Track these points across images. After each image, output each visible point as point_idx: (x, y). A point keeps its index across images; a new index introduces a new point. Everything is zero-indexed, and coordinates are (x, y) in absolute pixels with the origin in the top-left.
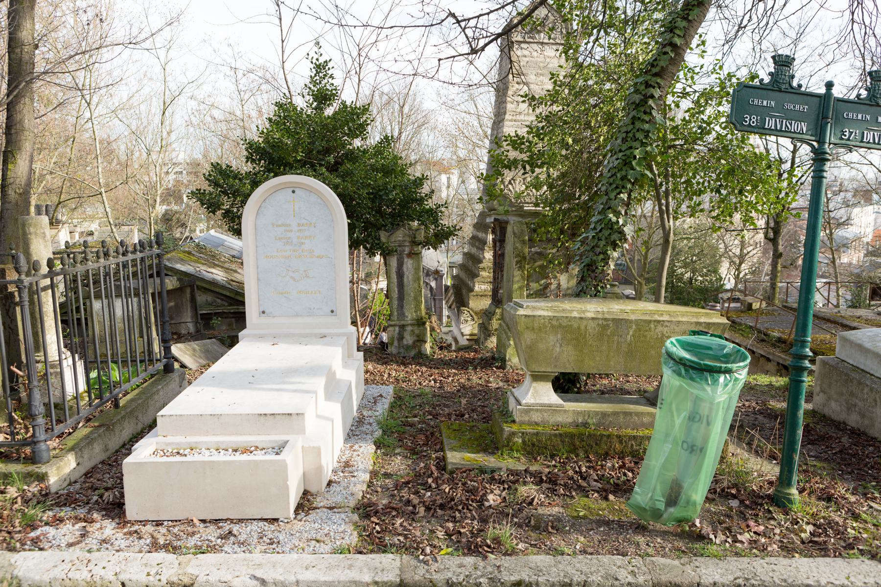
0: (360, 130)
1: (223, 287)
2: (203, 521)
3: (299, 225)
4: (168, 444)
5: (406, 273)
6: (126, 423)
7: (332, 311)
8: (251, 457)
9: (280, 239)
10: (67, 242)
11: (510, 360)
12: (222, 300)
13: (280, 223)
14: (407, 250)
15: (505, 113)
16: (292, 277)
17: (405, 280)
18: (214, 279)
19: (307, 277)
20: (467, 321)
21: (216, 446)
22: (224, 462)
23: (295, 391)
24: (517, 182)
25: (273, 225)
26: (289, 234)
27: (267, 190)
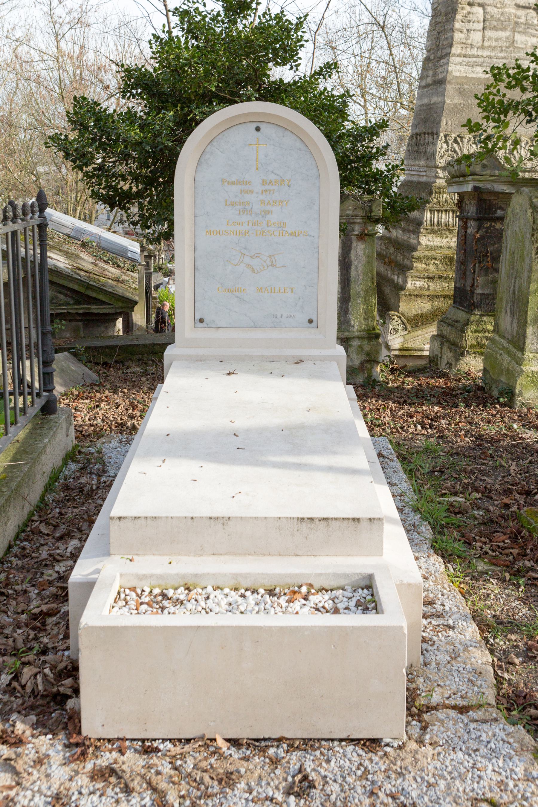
0: (288, 55)
1: (69, 278)
2: (235, 742)
3: (264, 182)
4: (143, 577)
5: (355, 263)
6: (11, 510)
7: (310, 321)
9: (233, 204)
10: (505, 87)
11: (521, 394)
12: (66, 295)
13: (234, 178)
14: (357, 230)
15: (451, 46)
16: (249, 266)
17: (353, 273)
18: (56, 267)
19: (273, 265)
20: (397, 330)
21: (232, 583)
22: (282, 629)
23: (330, 469)
24: (466, 141)
25: (223, 181)
26: (248, 197)
27: (220, 124)
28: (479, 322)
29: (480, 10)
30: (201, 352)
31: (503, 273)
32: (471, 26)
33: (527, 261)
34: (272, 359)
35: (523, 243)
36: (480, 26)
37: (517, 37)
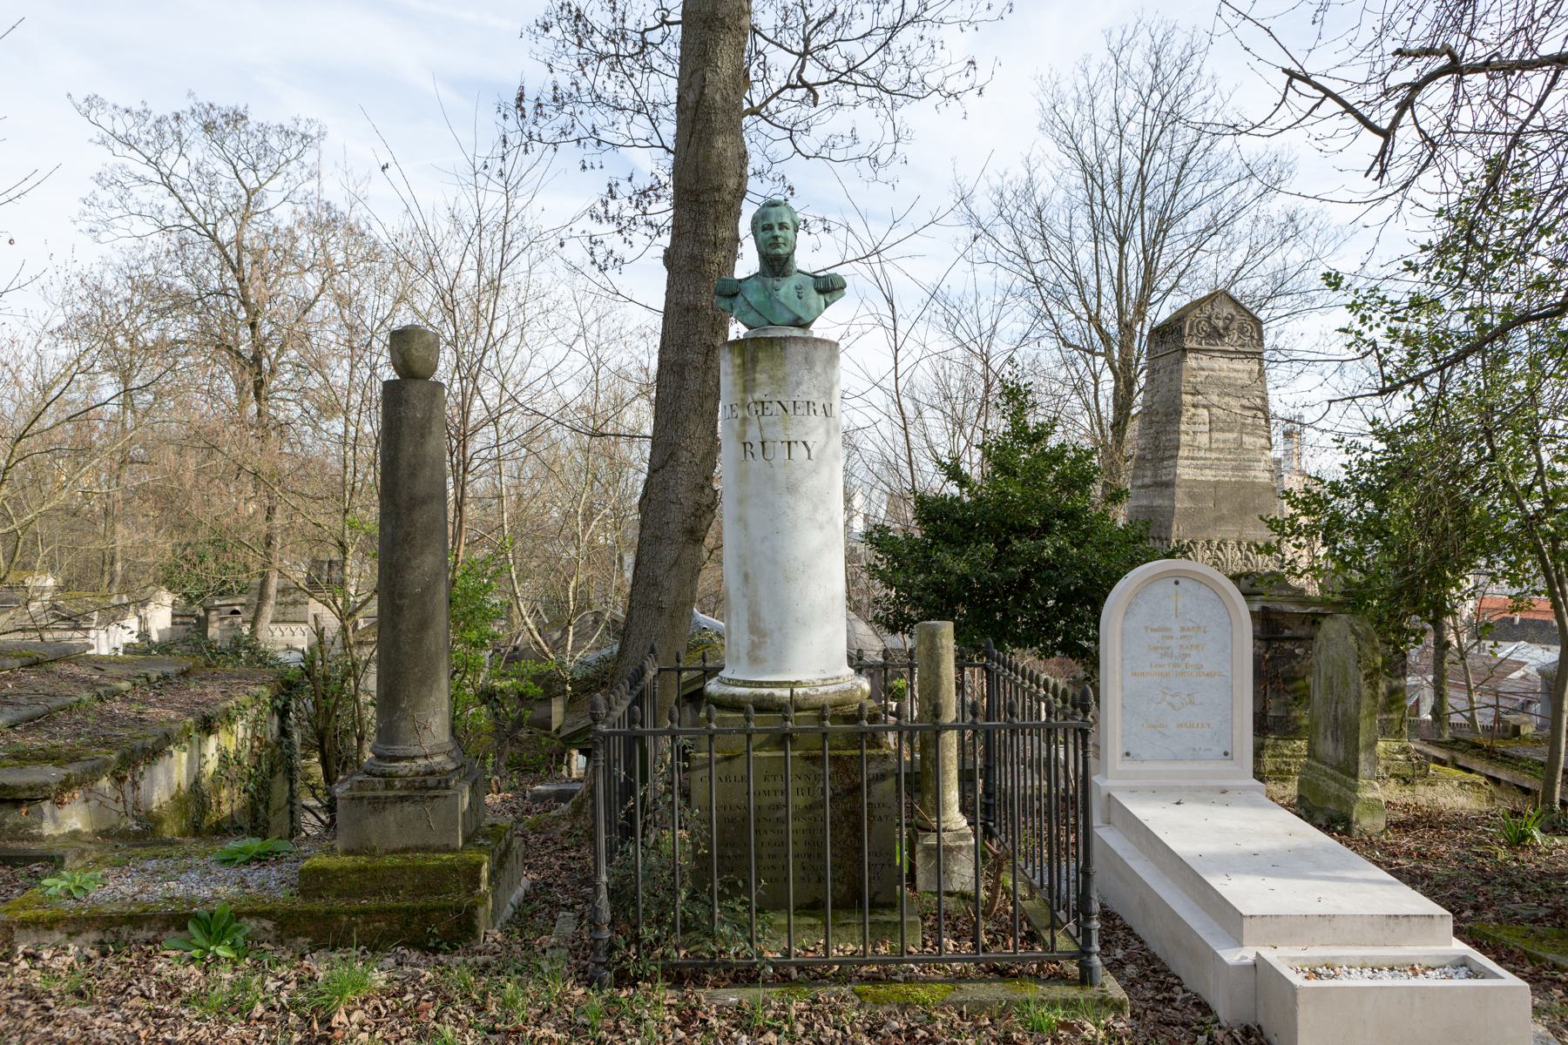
3: (1183, 629)
7: (1226, 754)
8: (1420, 981)
9: (1156, 648)
11: (1358, 822)
15: (1178, 448)
19: (1191, 703)
26: (1168, 642)
28: (1275, 746)
29: (1205, 412)
30: (1132, 783)
31: (1317, 696)
32: (1197, 428)
33: (1353, 687)
34: (1199, 790)
35: (1346, 669)
36: (1207, 428)
37: (1246, 438)
